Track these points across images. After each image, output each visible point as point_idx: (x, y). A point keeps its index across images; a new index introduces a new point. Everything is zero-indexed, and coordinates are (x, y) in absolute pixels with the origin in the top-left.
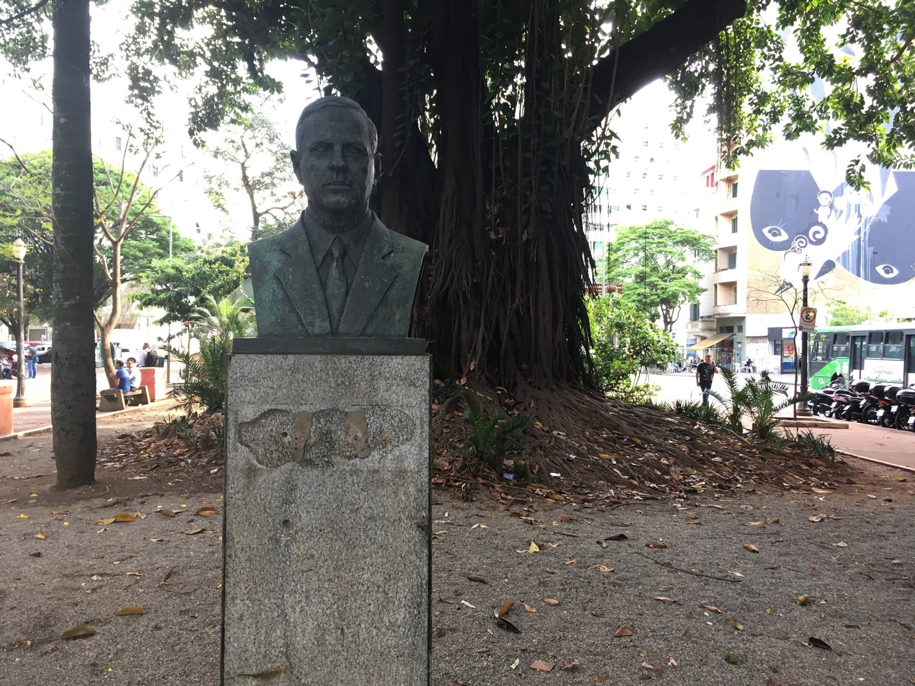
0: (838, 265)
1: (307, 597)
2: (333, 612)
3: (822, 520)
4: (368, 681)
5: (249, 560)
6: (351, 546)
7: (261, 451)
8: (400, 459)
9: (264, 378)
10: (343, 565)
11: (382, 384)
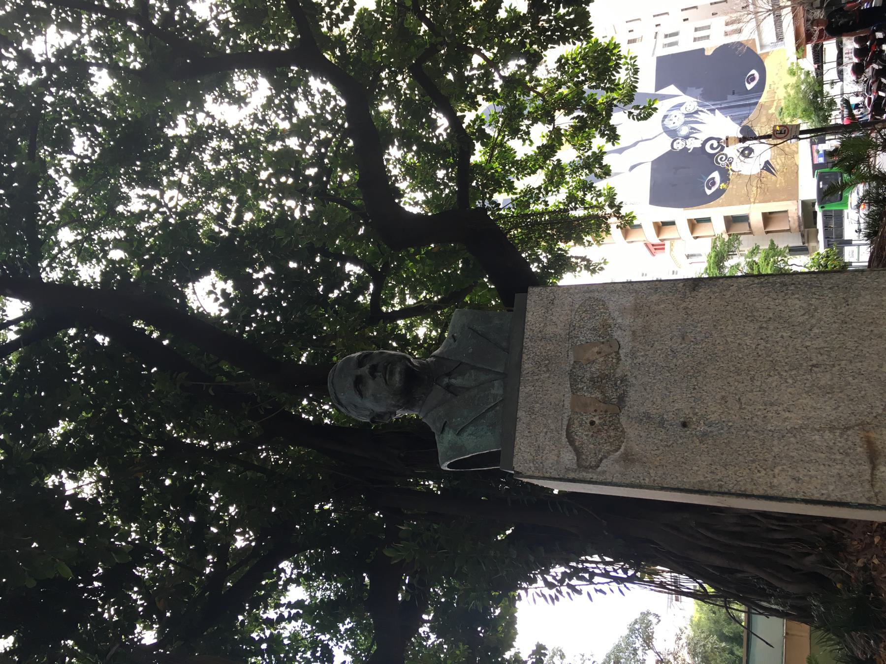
0: (745, 123)
1: (772, 404)
2: (791, 376)
4: (880, 337)
5: (725, 466)
7: (607, 447)
8: (623, 311)
9: (536, 441)
10: (733, 366)
11: (550, 330)
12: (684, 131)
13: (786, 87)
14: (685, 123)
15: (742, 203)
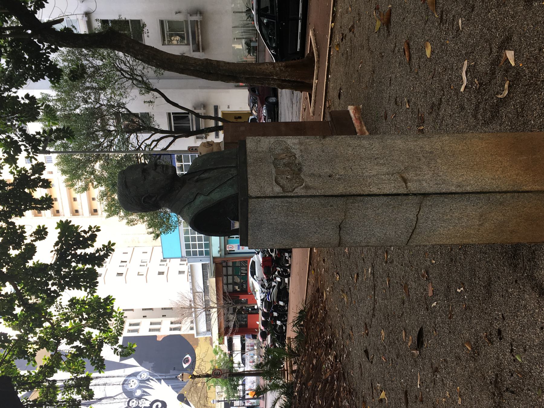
0: (181, 392)
1: (364, 169)
3: (338, 273)
11: (260, 150)
12: (138, 393)
13: (212, 361)
14: (140, 387)
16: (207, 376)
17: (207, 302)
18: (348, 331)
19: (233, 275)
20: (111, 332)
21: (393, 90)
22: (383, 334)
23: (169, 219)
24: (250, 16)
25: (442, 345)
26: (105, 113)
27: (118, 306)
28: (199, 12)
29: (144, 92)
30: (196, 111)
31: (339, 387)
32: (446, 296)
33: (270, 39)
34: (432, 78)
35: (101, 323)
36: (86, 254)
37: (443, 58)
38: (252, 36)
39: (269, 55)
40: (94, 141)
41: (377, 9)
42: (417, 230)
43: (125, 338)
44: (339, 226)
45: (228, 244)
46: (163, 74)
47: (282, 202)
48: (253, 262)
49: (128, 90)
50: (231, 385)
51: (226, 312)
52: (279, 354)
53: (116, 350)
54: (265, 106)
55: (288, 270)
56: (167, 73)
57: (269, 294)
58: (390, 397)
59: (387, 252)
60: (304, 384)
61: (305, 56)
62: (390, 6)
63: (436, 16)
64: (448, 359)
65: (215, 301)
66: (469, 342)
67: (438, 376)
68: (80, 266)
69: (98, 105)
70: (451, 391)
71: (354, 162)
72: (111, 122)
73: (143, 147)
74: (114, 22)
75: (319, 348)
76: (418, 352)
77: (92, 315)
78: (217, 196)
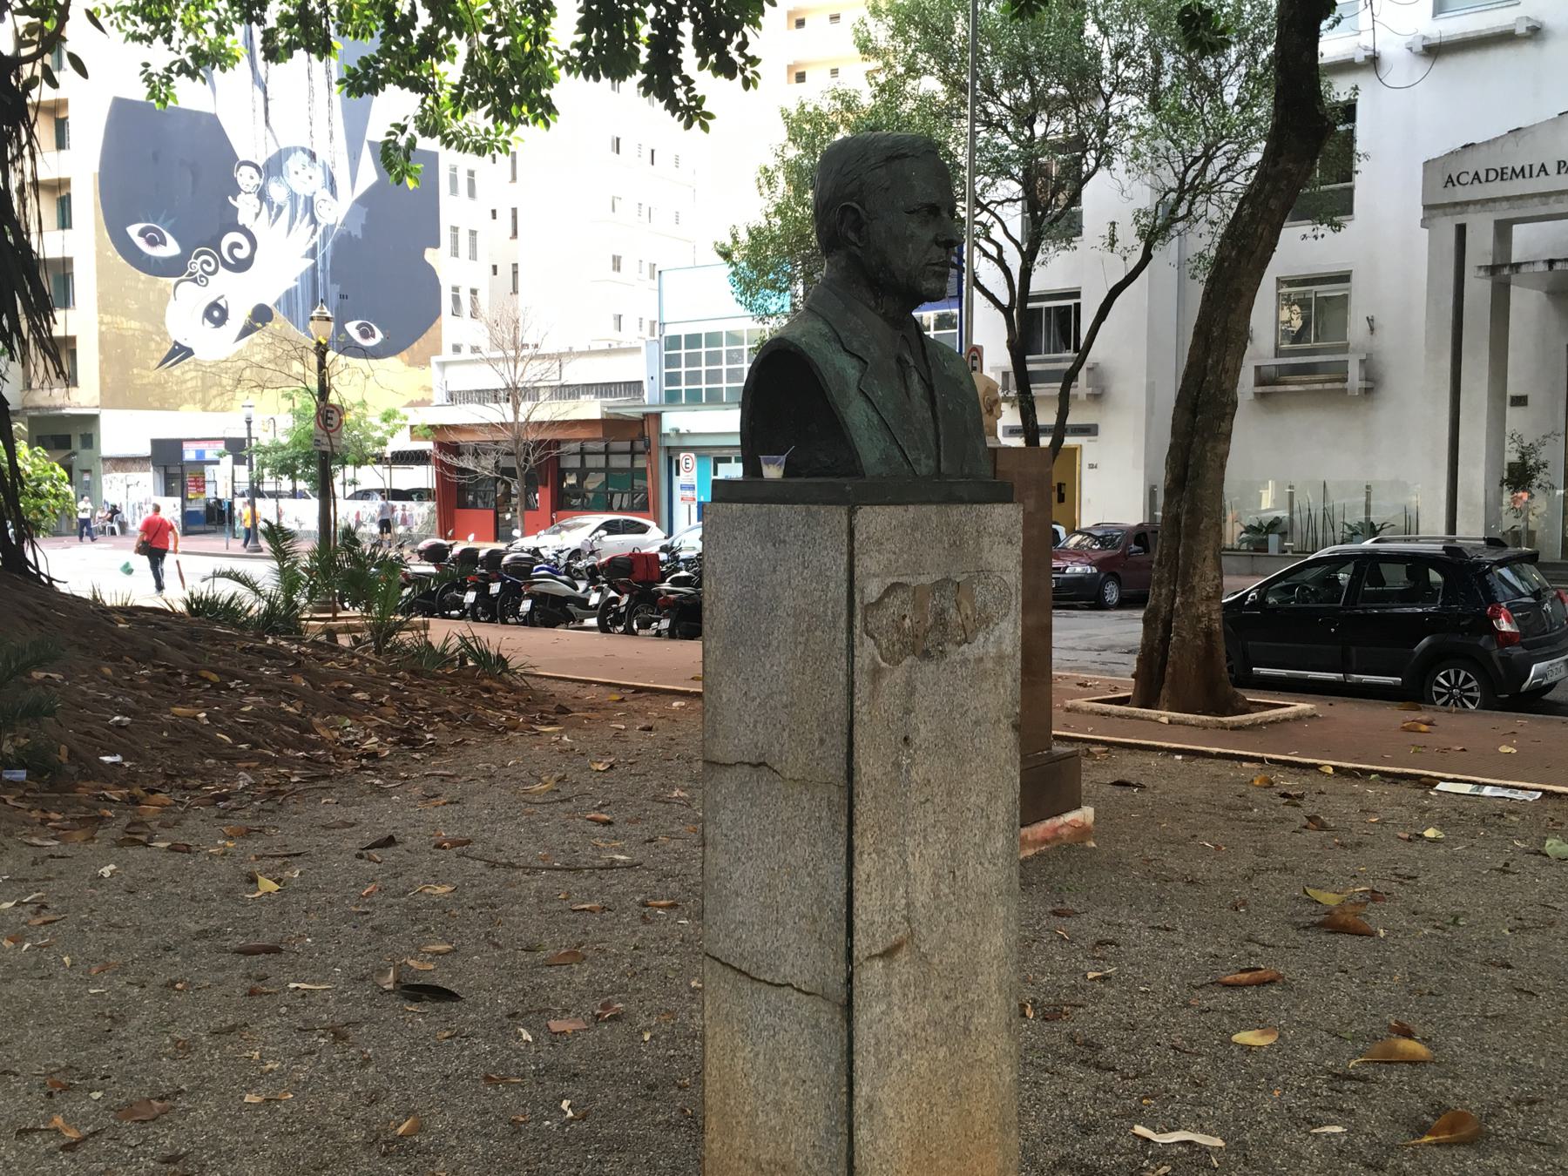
0: (278, 314)
3: (612, 767)
5: (875, 797)
6: (961, 762)
7: (884, 643)
11: (986, 541)
12: (277, 192)
13: (363, 404)
14: (293, 197)
15: (102, 297)
16: (324, 391)
17: (532, 393)
18: (449, 791)
19: (607, 470)
20: (454, 115)
21: (1138, 937)
22: (440, 890)
23: (773, 288)
24: (1355, 534)
25: (410, 1054)
26: (1084, 108)
27: (528, 137)
28: (1372, 386)
29: (1143, 221)
30: (1082, 373)
31: (291, 763)
32: (549, 1069)
33: (1288, 590)
34: (1173, 1047)
35: (481, 87)
36: (678, 46)
37: (1232, 1078)
38: (1297, 537)
39: (1242, 584)
40: (1005, 76)
41: (1375, 896)
42: (747, 986)
43: (433, 158)
44: (764, 764)
45: (698, 456)
46: (1194, 277)
47: (837, 602)
48: (643, 529)
49: (1149, 178)
50: (294, 459)
51: (503, 447)
52: (385, 597)
53: (403, 129)
54: (1095, 570)
55: (621, 629)
56: (1197, 290)
57: (554, 571)
58: (263, 904)
59: (673, 906)
60: (298, 663)
61: (1239, 691)
62: (1382, 933)
63: (1353, 1063)
64: (371, 1069)
65: (535, 417)
66: (420, 1129)
67: (322, 1040)
68: (645, 31)
69: (1107, 89)
70: (280, 1076)
71: (944, 810)
72: (1058, 125)
73: (984, 217)
74: (1350, 137)
75: (399, 709)
76: (390, 987)
77: (504, 63)
78: (857, 415)
